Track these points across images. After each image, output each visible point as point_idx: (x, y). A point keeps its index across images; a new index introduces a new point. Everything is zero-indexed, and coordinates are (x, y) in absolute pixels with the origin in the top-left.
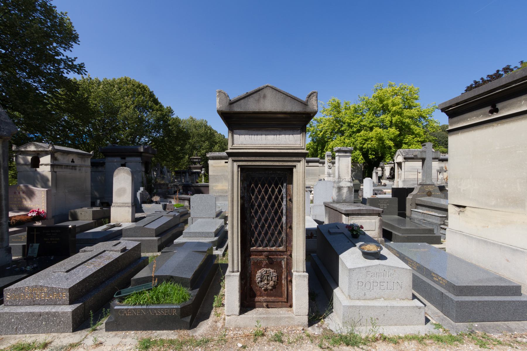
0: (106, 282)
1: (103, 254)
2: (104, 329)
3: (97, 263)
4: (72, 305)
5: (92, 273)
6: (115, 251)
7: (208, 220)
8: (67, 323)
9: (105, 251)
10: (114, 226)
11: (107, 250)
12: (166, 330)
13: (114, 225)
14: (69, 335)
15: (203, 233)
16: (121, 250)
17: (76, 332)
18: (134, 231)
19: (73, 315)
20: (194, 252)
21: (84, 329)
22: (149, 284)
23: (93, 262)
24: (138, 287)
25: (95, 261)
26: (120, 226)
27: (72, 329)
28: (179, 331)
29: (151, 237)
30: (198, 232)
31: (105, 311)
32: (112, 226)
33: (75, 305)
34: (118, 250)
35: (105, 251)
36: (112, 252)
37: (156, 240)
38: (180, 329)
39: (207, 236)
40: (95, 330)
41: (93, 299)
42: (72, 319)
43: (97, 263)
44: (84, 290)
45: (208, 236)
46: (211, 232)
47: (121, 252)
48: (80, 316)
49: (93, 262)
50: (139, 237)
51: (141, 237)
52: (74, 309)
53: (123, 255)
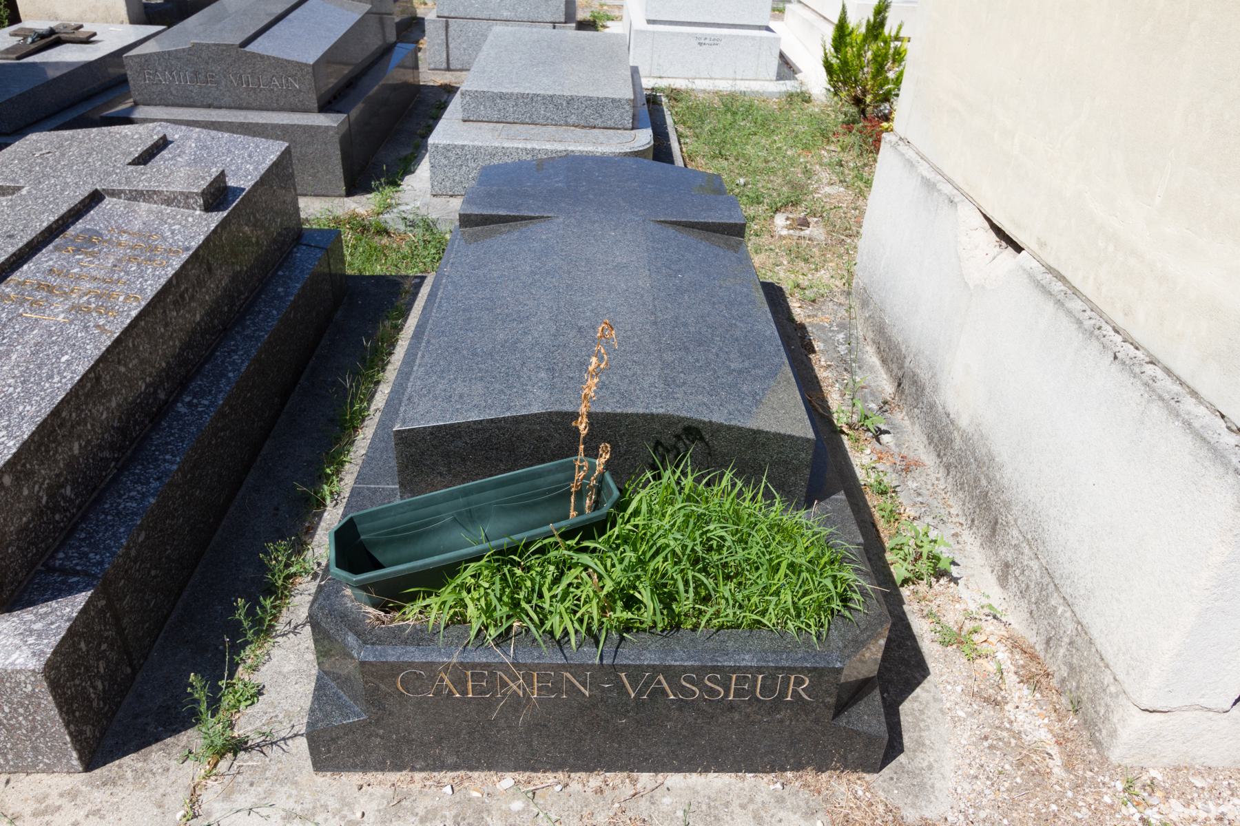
0: (181, 408)
1: (92, 220)
2: (301, 746)
3: (86, 285)
4: (28, 615)
5: (81, 369)
6: (169, 201)
7: (525, 31)
8: (34, 729)
9: (95, 198)
10: (51, 39)
11: (114, 194)
12: (721, 769)
13: (52, 32)
14: (73, 795)
15: (570, 100)
16: (203, 194)
17: (113, 766)
18: (196, 73)
19: (56, 686)
20: (671, 231)
21: (157, 740)
22: (538, 475)
23: (52, 280)
24: (466, 493)
25: (63, 273)
26: (88, 40)
27: (80, 758)
28: (809, 778)
29: (293, 110)
30: (544, 97)
31: (250, 613)
32: (42, 36)
33: (42, 609)
34: (187, 196)
35: (95, 198)
36: (144, 206)
37: (327, 128)
38: (820, 769)
39: (592, 122)
40: (237, 746)
41: (147, 538)
42: (60, 706)
43: (86, 285)
44: (68, 491)
45: (599, 122)
46: (613, 100)
47: (208, 208)
48: (102, 665)
49: (52, 280)
50: (230, 108)
51: (240, 108)
52: (49, 645)
53: (223, 224)
